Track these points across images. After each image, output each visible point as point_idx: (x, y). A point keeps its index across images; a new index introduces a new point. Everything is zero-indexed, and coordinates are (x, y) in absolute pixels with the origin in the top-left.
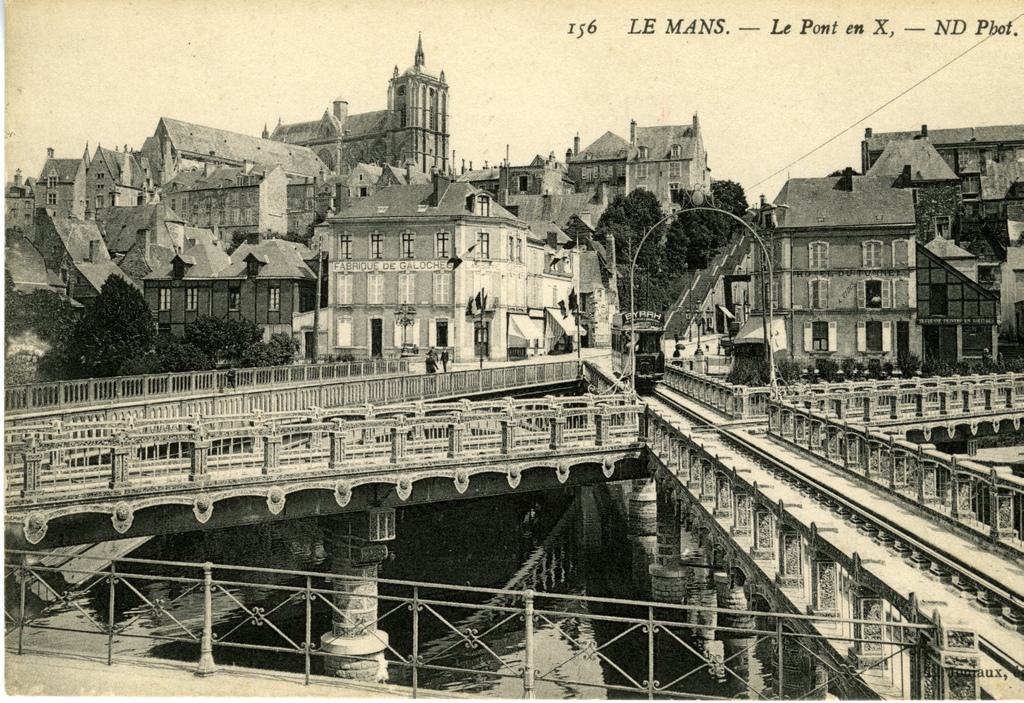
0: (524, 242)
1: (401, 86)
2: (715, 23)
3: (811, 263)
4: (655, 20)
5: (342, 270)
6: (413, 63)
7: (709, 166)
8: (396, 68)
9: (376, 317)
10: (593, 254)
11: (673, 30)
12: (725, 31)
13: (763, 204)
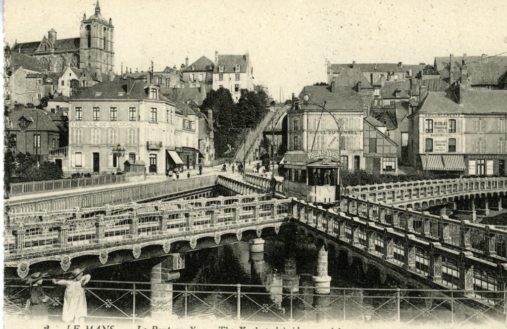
0: (173, 114)
5: (77, 126)
6: (94, 13)
7: (253, 76)
8: (85, 15)
9: (96, 151)
10: (203, 119)
13: (293, 98)
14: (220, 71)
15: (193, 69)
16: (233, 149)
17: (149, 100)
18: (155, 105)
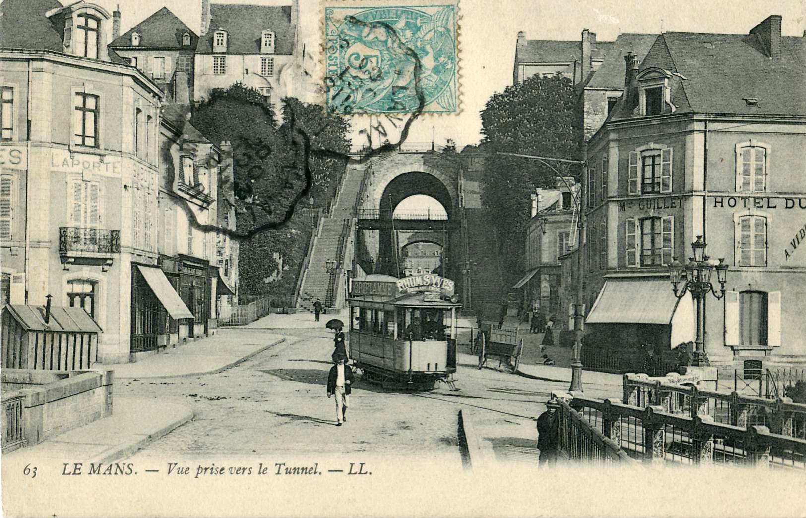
1: (283, 101)
2: (126, 466)
3: (740, 182)
4: (81, 465)
11: (94, 472)
12: (134, 472)
14: (218, 49)
15: (136, 42)
16: (286, 268)
17: (70, 61)
18: (92, 82)
